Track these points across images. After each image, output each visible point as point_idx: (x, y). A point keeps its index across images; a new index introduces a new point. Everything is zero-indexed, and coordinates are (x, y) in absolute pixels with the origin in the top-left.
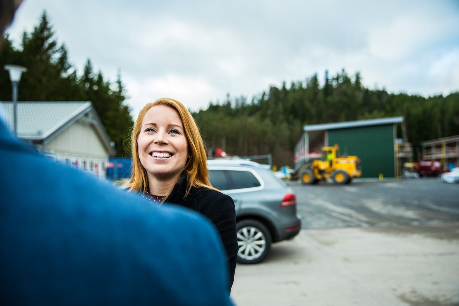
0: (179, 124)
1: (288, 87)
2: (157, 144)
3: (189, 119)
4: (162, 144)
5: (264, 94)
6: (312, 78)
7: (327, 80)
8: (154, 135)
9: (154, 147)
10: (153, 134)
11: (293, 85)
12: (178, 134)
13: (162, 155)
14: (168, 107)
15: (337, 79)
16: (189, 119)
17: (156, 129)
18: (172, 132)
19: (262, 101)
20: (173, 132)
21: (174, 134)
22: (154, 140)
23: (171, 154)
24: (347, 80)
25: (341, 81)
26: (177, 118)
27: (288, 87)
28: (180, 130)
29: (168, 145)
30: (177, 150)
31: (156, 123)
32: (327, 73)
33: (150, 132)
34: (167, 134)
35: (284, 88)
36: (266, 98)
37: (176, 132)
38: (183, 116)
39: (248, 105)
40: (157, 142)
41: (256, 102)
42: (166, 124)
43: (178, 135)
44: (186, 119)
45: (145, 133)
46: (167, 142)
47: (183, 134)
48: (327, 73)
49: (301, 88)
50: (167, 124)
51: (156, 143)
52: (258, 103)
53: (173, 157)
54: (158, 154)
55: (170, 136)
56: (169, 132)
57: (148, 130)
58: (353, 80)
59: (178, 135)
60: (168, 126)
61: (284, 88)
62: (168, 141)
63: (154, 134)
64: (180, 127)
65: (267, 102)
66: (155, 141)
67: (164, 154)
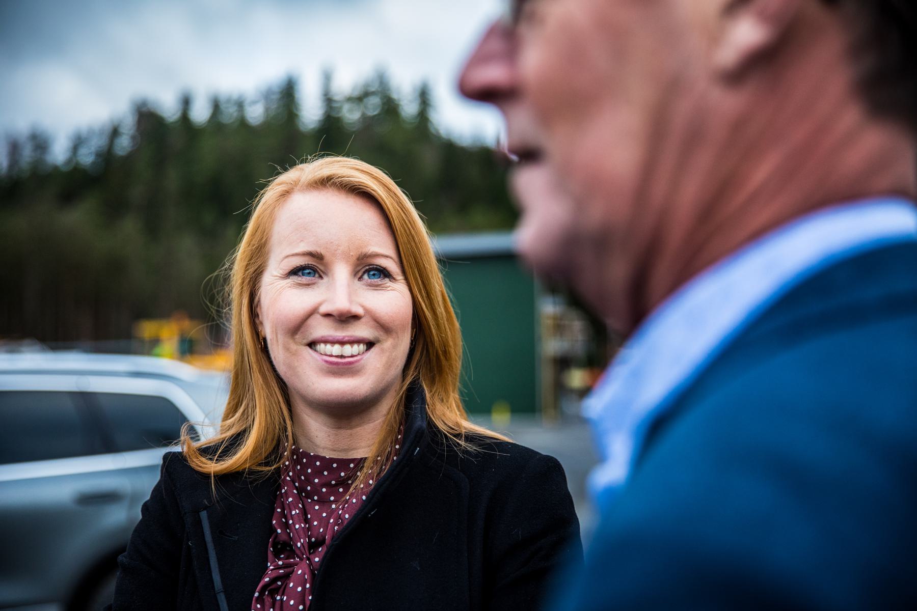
0: (389, 250)
1: (200, 113)
2: (332, 318)
3: (413, 229)
4: (346, 318)
5: (115, 132)
6: (281, 92)
7: (328, 100)
8: (315, 287)
9: (321, 329)
10: (314, 284)
11: (216, 106)
12: (387, 280)
13: (348, 350)
14: (353, 196)
15: (360, 98)
16: (413, 229)
17: (322, 268)
18: (372, 273)
19: (107, 156)
20: (374, 275)
21: (377, 281)
22: (320, 304)
23: (370, 344)
24: (390, 107)
25: (373, 105)
26: (381, 231)
27: (200, 113)
28: (392, 265)
29: (363, 320)
30: (385, 328)
31: (323, 252)
32: (327, 78)
33: (305, 279)
34: (356, 281)
35: (185, 117)
36: (124, 144)
37: (384, 273)
38: (397, 223)
39: (56, 168)
40: (334, 314)
41: (87, 158)
42: (351, 254)
43: (388, 285)
44: (405, 231)
45: (288, 281)
46: (359, 311)
47: (400, 277)
48: (327, 78)
49: (243, 123)
50: (354, 253)
51: (328, 315)
52: (93, 163)
53: (374, 350)
54: (336, 349)
55: (365, 287)
56: (360, 274)
57: (295, 272)
58: (409, 108)
59: (388, 285)
60: (358, 259)
61: (185, 117)
62: (363, 306)
63: (316, 285)
64: (391, 258)
65: (130, 158)
66: (324, 309)
67: (358, 346)
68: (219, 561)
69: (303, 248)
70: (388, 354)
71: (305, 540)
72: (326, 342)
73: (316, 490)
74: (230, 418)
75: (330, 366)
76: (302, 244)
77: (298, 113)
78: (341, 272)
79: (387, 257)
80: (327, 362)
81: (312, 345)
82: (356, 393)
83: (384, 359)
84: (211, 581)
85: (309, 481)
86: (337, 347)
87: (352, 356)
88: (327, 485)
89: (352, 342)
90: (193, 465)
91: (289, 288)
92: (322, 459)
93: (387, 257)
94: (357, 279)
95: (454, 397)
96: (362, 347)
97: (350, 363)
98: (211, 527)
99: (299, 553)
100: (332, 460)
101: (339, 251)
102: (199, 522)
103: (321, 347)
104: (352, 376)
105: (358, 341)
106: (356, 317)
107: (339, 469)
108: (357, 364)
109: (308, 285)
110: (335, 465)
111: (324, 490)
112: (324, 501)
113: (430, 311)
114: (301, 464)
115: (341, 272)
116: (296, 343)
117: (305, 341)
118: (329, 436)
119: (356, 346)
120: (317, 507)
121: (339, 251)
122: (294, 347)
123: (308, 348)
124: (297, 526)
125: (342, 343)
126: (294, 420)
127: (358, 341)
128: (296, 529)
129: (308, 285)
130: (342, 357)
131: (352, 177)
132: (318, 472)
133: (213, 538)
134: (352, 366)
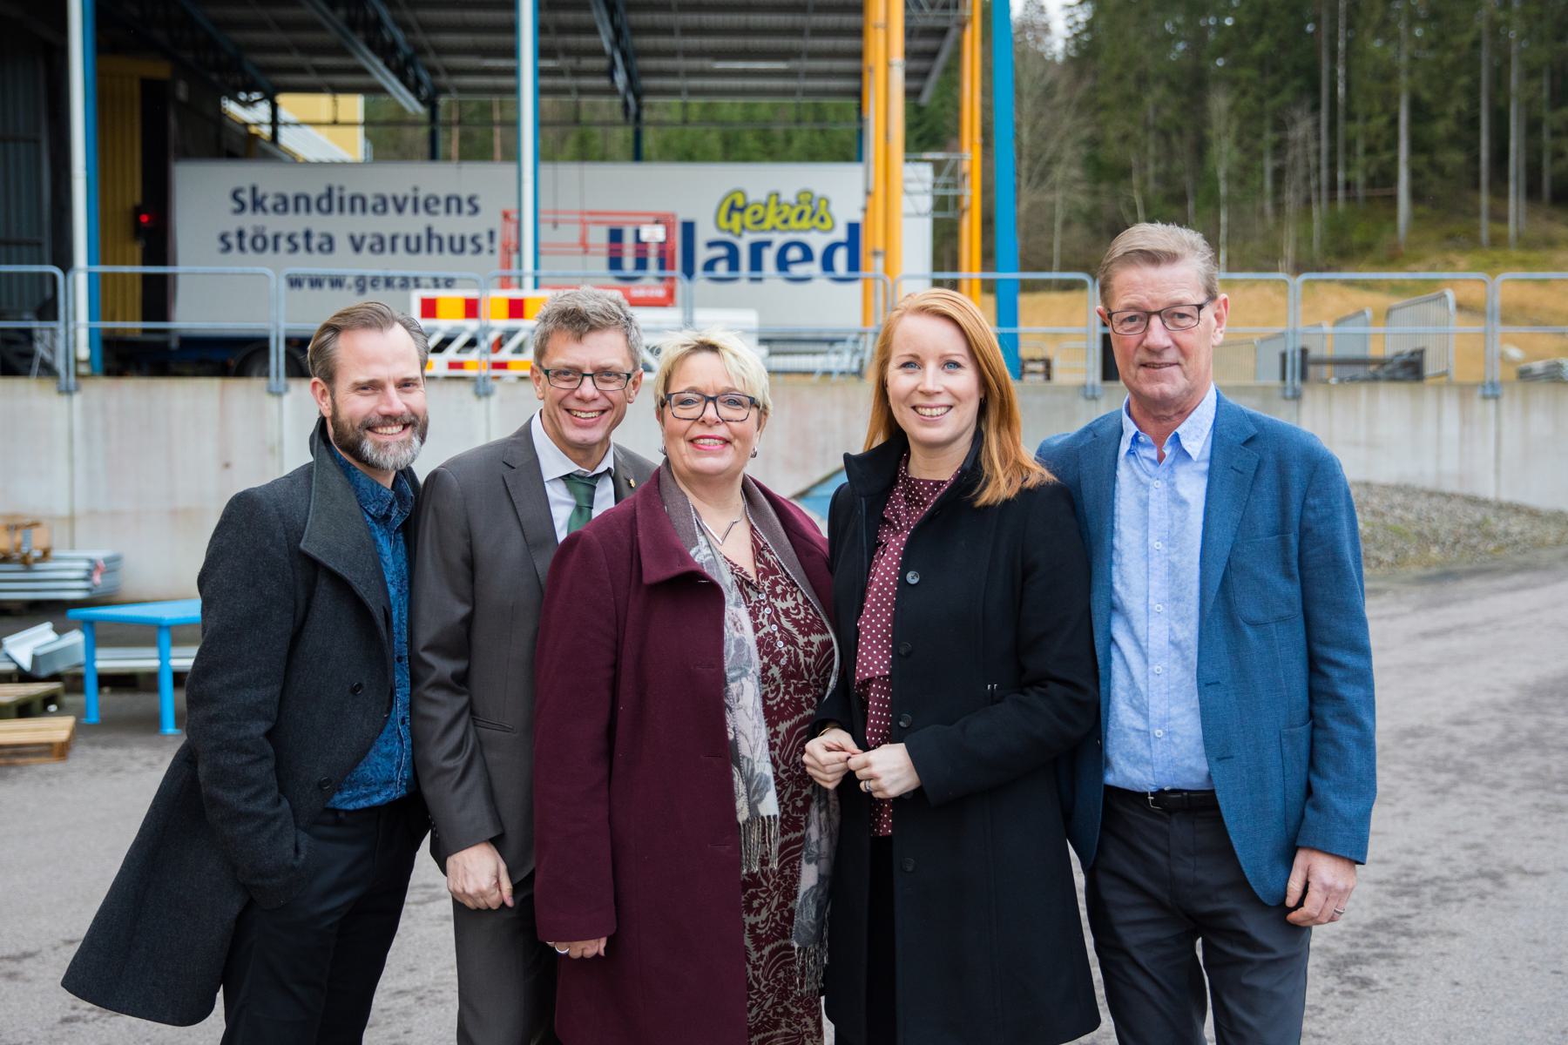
21: (952, 370)
22: (918, 385)
29: (944, 394)
33: (910, 370)
37: (957, 365)
46: (940, 389)
50: (937, 355)
53: (953, 410)
57: (905, 365)
66: (920, 388)
69: (911, 352)
72: (922, 407)
74: (568, 381)
78: (931, 367)
87: (938, 416)
90: (1199, 235)
92: (915, 480)
96: (944, 410)
103: (920, 410)
105: (941, 406)
107: (924, 486)
109: (912, 373)
113: (796, 515)
114: (911, 494)
115: (931, 367)
126: (146, 597)
127: (941, 406)
130: (932, 416)
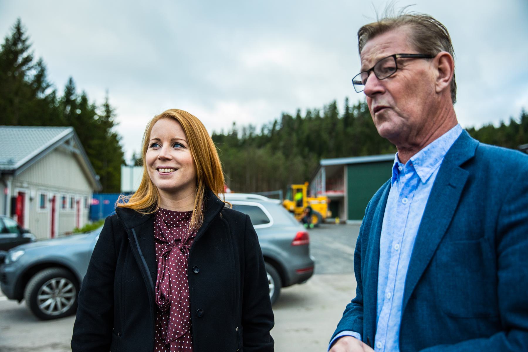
0: (184, 138)
1: (303, 115)
4: (164, 159)
5: (276, 123)
9: (159, 164)
11: (309, 113)
13: (166, 170)
19: (273, 131)
23: (176, 169)
28: (184, 143)
31: (160, 138)
35: (298, 116)
36: (278, 128)
37: (182, 146)
46: (170, 157)
49: (318, 117)
50: (170, 138)
60: (171, 140)
61: (298, 116)
62: (172, 156)
65: (279, 132)
68: (140, 245)
70: (182, 173)
71: (173, 241)
73: (175, 223)
75: (161, 175)
76: (155, 136)
77: (338, 112)
78: (166, 144)
79: (182, 140)
80: (160, 174)
81: (158, 169)
82: (170, 185)
83: (181, 174)
84: (138, 252)
85: (172, 219)
86: (163, 169)
88: (179, 221)
89: (168, 168)
91: (399, 181)
93: (182, 140)
94: (172, 147)
95: (228, 190)
97: (167, 174)
98: (136, 234)
99: (172, 245)
100: (174, 212)
101: (165, 138)
102: (132, 232)
104: (168, 179)
105: (171, 168)
106: (168, 160)
108: (170, 175)
110: (180, 214)
111: (177, 223)
112: (177, 226)
115: (166, 144)
116: (152, 169)
117: (155, 168)
118: (171, 202)
119: (169, 169)
120: (175, 228)
121: (165, 138)
122: (152, 170)
123: (156, 170)
124: (170, 236)
125: (165, 168)
128: (170, 238)
129: (157, 149)
131: (171, 113)
132: (175, 217)
133: (137, 238)
134: (168, 175)
